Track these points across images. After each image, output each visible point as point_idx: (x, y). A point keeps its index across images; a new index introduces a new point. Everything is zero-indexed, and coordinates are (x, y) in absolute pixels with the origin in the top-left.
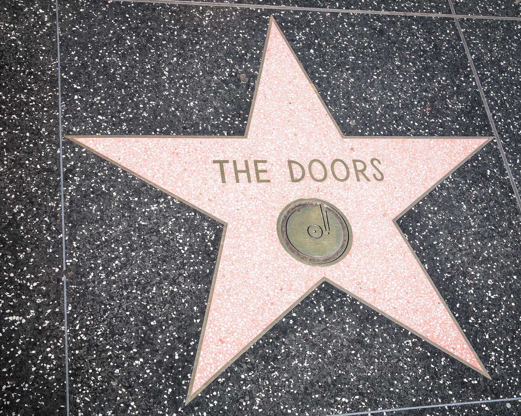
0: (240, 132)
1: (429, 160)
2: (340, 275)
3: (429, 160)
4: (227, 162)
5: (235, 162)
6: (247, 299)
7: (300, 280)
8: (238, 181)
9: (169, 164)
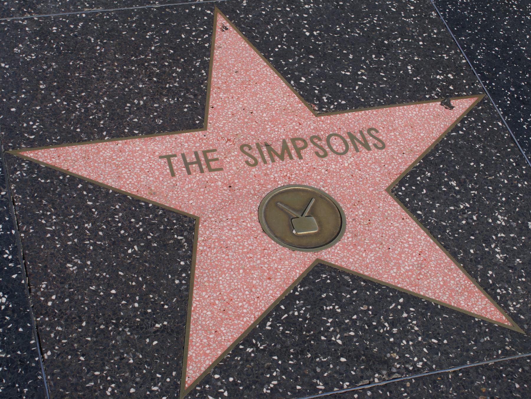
0: (202, 126)
1: (418, 126)
2: (334, 255)
3: (418, 126)
4: (175, 156)
5: (184, 156)
6: (235, 287)
7: (293, 265)
8: (189, 173)
9: (128, 165)
